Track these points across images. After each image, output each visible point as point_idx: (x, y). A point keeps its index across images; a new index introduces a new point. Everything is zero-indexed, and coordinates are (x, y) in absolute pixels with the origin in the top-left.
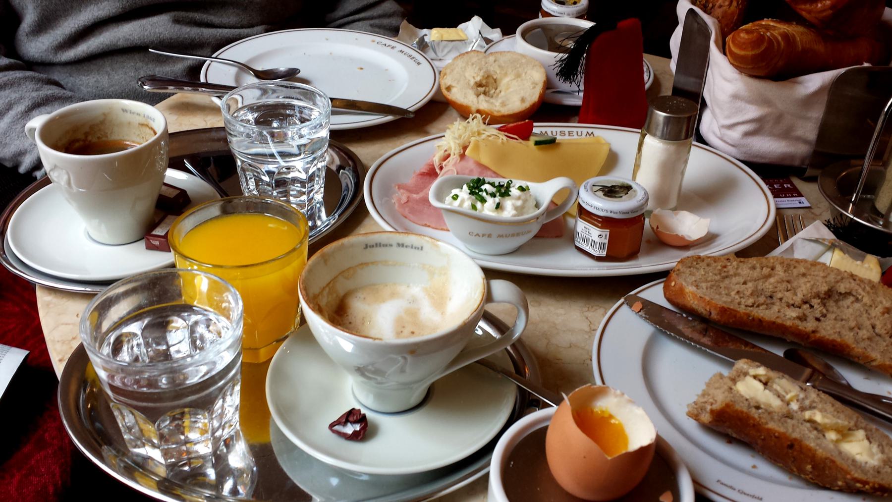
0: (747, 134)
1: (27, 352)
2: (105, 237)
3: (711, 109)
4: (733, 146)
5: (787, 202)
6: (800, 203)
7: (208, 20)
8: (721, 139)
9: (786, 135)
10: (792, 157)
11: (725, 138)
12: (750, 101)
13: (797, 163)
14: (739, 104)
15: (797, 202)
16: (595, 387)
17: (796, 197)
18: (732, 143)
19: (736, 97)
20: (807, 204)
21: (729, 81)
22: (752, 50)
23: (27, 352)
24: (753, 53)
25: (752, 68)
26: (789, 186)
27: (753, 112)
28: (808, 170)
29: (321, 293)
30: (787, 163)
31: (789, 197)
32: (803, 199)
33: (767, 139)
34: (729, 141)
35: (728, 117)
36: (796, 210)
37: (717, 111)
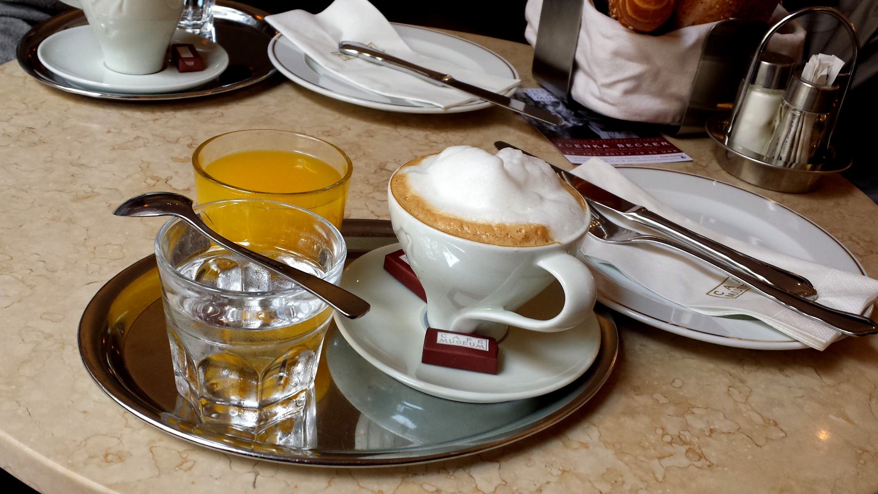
0: (627, 92)
1: (400, 257)
2: (125, 69)
3: (504, 93)
4: (613, 105)
5: (670, 157)
6: (682, 157)
7: (9, 38)
8: (602, 99)
9: (660, 94)
10: (665, 114)
11: (606, 98)
12: (630, 59)
13: (669, 121)
14: (621, 61)
15: (680, 157)
16: (269, 327)
17: (675, 152)
18: (612, 102)
19: (617, 54)
20: (688, 158)
21: (609, 38)
22: (655, 5)
23: (400, 257)
24: (656, 7)
25: (649, 23)
26: (666, 143)
27: (635, 69)
28: (681, 128)
29: (13, 276)
30: (660, 121)
31: (670, 153)
32: (683, 154)
33: (644, 96)
34: (609, 100)
35: (607, 75)
36: (686, 163)
37: (596, 70)
